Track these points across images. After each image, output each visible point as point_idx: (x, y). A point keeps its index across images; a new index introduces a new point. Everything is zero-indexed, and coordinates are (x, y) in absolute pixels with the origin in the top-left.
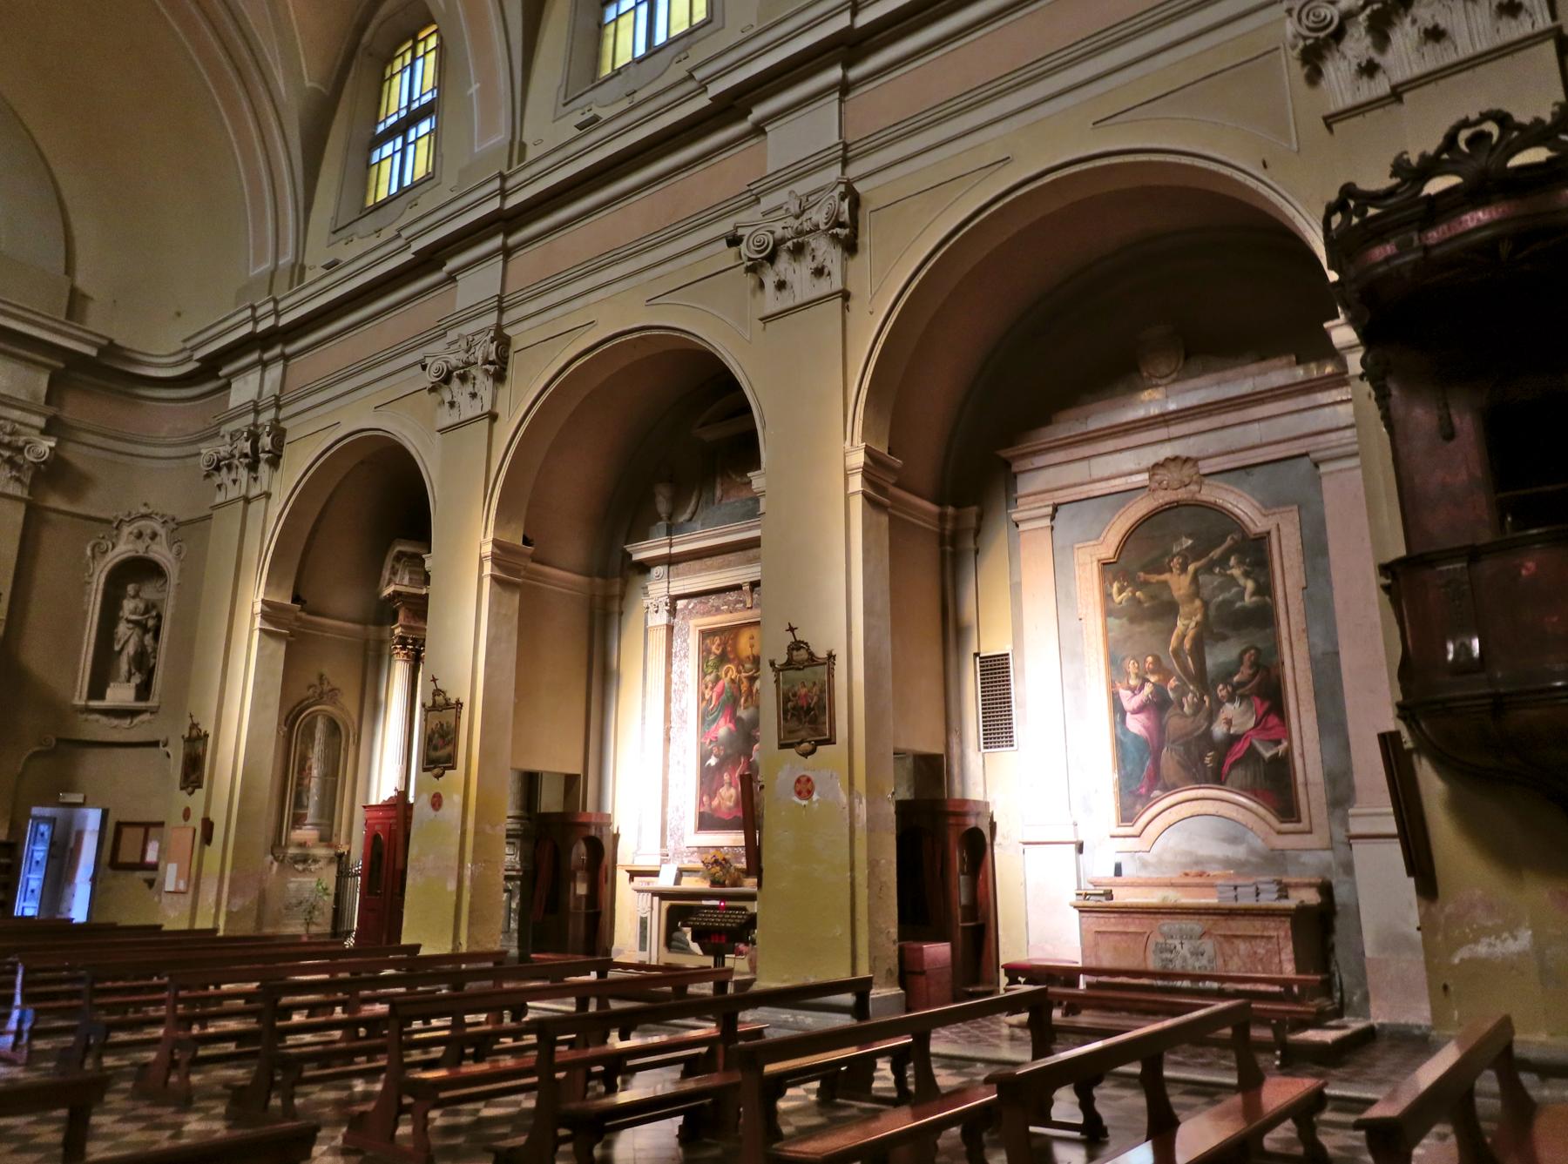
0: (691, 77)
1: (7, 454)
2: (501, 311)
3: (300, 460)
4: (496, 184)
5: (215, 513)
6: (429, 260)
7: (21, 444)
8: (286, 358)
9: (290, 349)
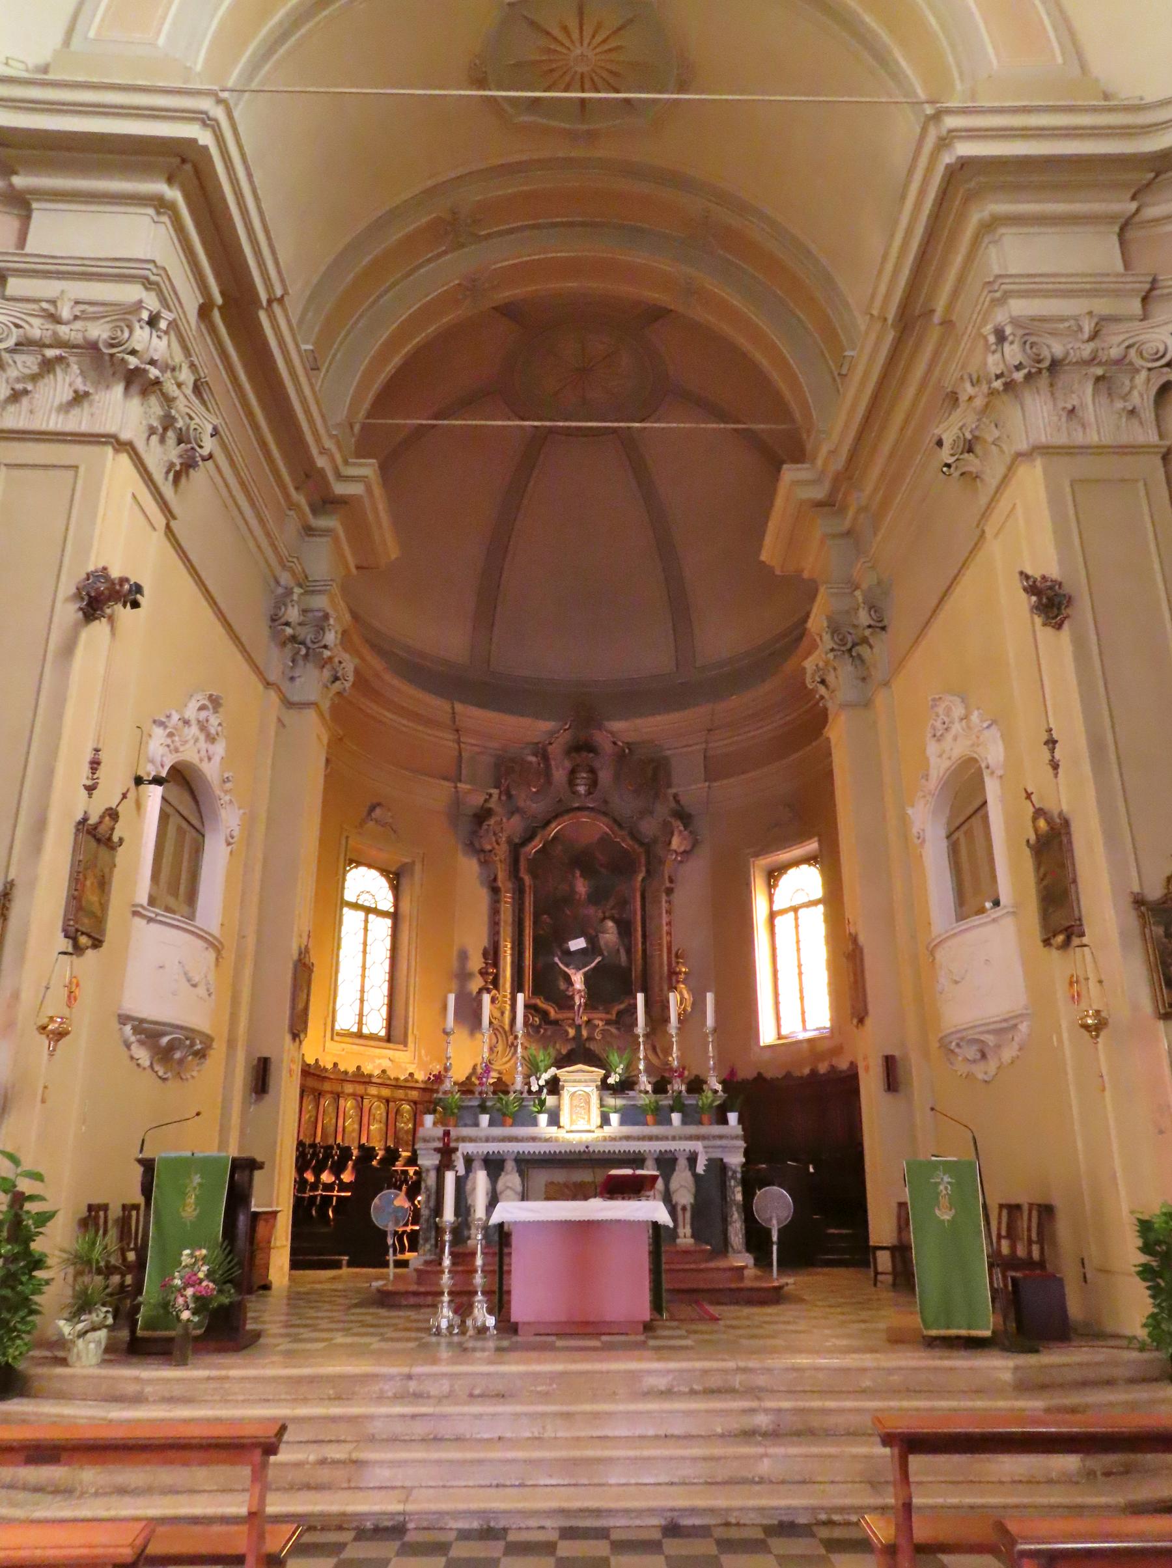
7: (1115, 353)
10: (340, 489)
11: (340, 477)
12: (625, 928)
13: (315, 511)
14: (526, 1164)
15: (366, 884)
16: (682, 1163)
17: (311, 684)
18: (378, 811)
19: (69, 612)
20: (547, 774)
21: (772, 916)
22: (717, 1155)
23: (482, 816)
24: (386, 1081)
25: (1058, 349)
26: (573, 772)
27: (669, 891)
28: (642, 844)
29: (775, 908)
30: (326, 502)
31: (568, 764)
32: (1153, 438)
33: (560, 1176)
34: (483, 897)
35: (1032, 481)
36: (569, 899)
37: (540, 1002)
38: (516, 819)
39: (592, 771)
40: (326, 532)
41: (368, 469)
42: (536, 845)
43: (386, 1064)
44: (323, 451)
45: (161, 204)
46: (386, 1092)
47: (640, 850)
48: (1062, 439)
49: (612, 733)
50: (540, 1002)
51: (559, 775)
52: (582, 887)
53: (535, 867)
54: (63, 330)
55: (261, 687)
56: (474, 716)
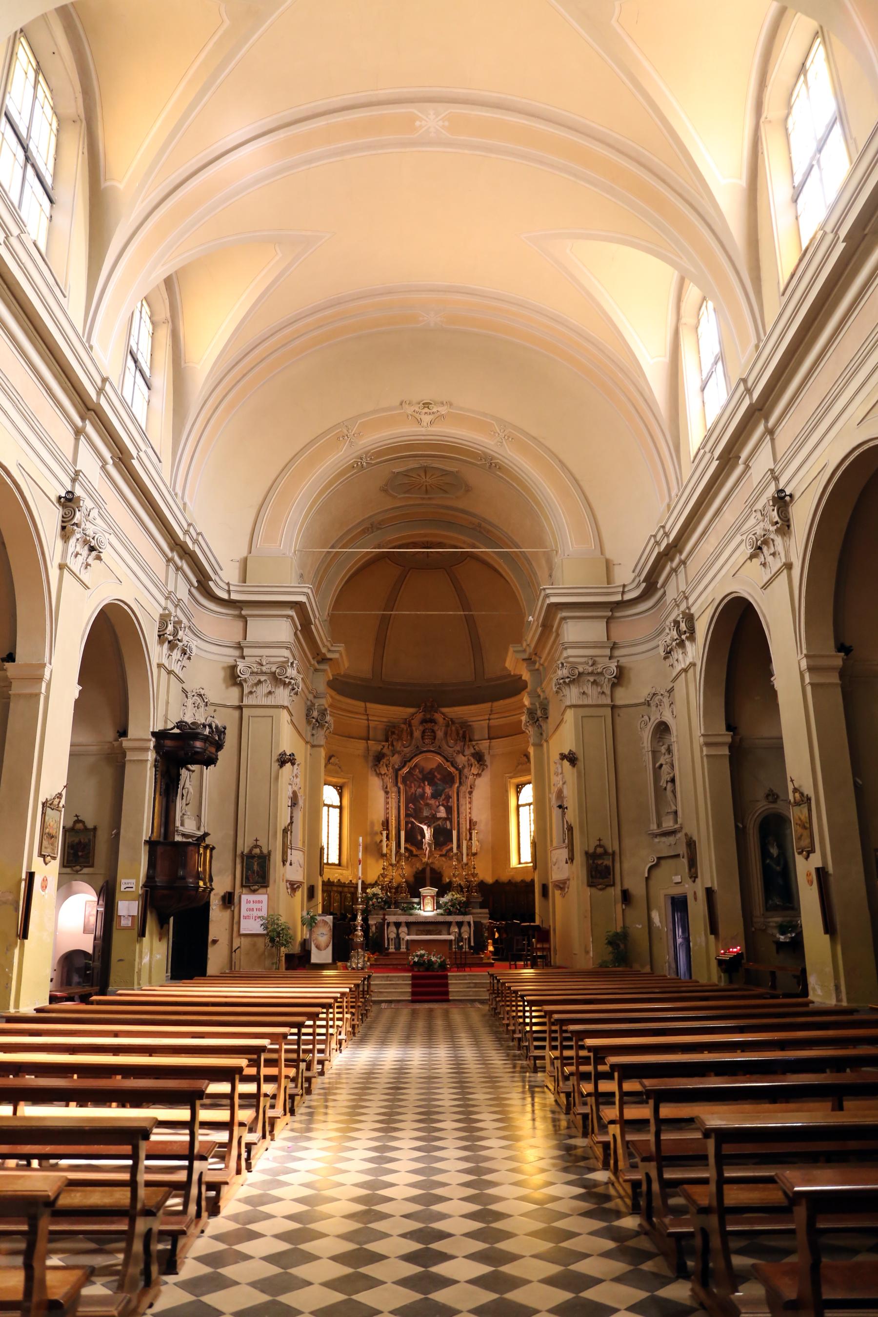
0: (198, 534)
1: (592, 679)
2: (776, 479)
3: (702, 627)
4: (742, 388)
5: (675, 684)
6: (729, 458)
7: (599, 670)
8: (683, 562)
9: (683, 557)
10: (329, 656)
11: (329, 651)
12: (449, 810)
13: (318, 662)
14: (408, 924)
15: (330, 795)
16: (466, 924)
17: (321, 737)
18: (333, 759)
19: (276, 765)
20: (411, 734)
21: (518, 806)
22: (478, 920)
23: (379, 758)
24: (340, 884)
25: (581, 670)
26: (424, 732)
27: (470, 793)
28: (457, 769)
29: (520, 803)
30: (323, 660)
31: (421, 728)
32: (609, 701)
33: (421, 928)
34: (382, 794)
35: (570, 715)
36: (423, 796)
37: (408, 846)
38: (396, 756)
39: (433, 731)
40: (324, 671)
41: (341, 647)
42: (406, 770)
43: (340, 877)
44: (324, 646)
45: (288, 616)
46: (340, 889)
47: (457, 772)
48: (581, 703)
49: (443, 714)
50: (408, 846)
51: (417, 734)
52: (428, 790)
53: (404, 781)
54: (264, 669)
55: (304, 743)
56: (376, 708)
